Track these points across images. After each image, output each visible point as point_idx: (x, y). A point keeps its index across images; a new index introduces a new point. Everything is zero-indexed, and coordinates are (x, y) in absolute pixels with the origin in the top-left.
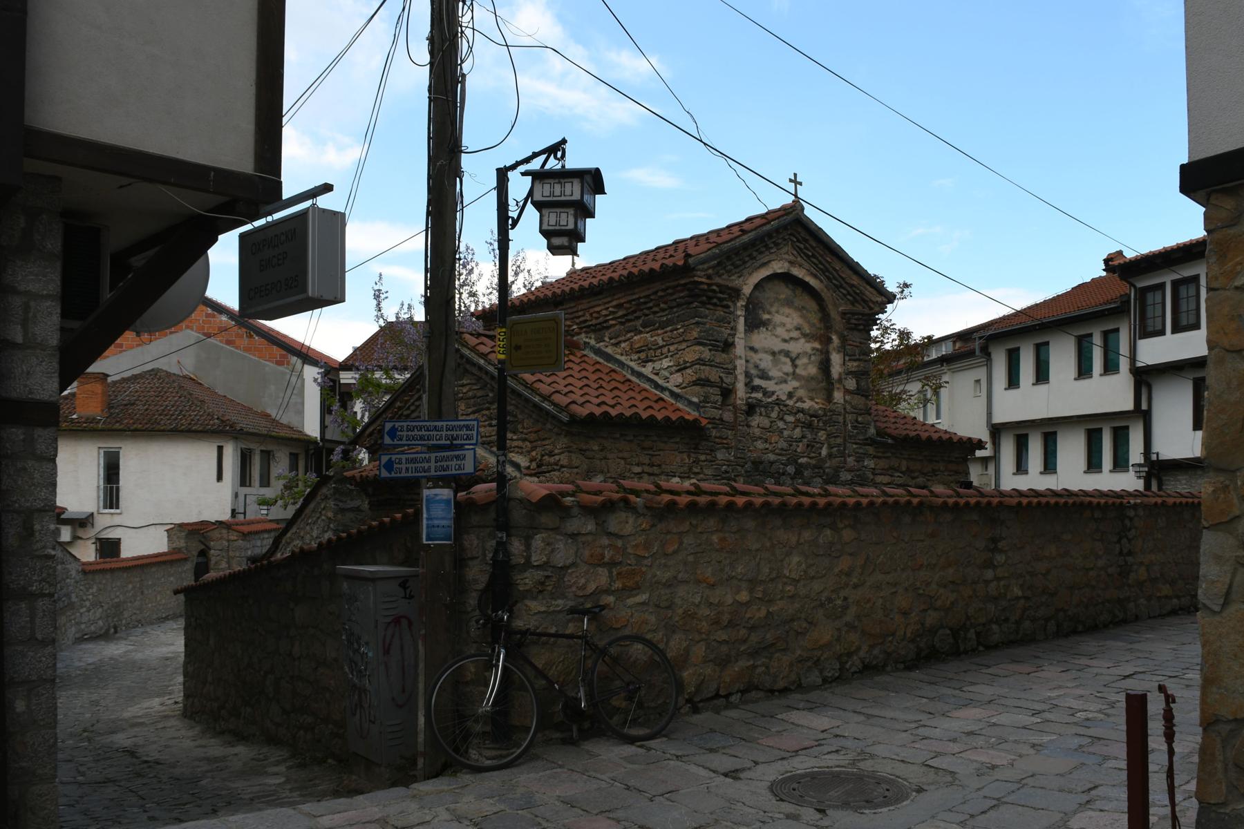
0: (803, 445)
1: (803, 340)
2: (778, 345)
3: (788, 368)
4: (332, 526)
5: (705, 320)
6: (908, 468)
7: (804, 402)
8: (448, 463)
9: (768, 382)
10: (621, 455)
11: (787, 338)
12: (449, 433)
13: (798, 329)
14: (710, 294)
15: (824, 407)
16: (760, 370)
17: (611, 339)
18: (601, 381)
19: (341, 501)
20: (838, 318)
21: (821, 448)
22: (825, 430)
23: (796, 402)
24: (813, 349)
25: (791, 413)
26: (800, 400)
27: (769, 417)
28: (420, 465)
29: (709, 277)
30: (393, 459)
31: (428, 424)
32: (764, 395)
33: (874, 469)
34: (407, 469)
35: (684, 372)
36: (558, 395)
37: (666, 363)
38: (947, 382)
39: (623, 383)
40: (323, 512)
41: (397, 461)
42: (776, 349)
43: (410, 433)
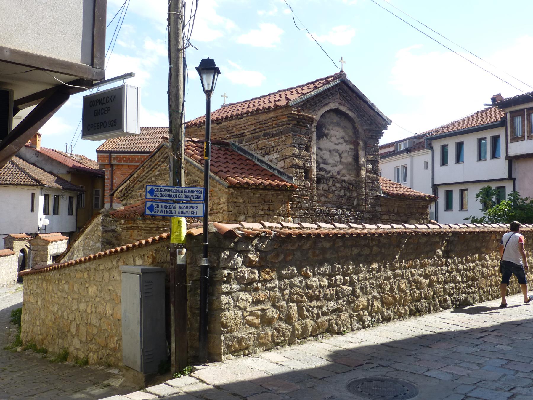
0: (345, 199)
1: (345, 144)
2: (332, 147)
3: (337, 158)
4: (100, 239)
5: (296, 134)
6: (398, 211)
7: (345, 176)
8: (187, 210)
9: (327, 166)
10: (253, 205)
11: (337, 143)
12: (186, 194)
13: (342, 138)
14: (299, 120)
15: (355, 179)
16: (324, 160)
17: (246, 142)
18: (242, 165)
19: (105, 226)
20: (363, 132)
21: (354, 201)
23: (342, 176)
24: (350, 148)
25: (338, 182)
26: (344, 175)
27: (328, 184)
28: (169, 209)
29: (298, 111)
30: (154, 205)
31: (174, 188)
32: (325, 172)
33: (381, 212)
34: (162, 211)
35: (285, 160)
36: (221, 172)
37: (275, 156)
38: (476, 200)
39: (253, 166)
40: (96, 232)
41: (156, 206)
42: (332, 149)
43: (162, 193)
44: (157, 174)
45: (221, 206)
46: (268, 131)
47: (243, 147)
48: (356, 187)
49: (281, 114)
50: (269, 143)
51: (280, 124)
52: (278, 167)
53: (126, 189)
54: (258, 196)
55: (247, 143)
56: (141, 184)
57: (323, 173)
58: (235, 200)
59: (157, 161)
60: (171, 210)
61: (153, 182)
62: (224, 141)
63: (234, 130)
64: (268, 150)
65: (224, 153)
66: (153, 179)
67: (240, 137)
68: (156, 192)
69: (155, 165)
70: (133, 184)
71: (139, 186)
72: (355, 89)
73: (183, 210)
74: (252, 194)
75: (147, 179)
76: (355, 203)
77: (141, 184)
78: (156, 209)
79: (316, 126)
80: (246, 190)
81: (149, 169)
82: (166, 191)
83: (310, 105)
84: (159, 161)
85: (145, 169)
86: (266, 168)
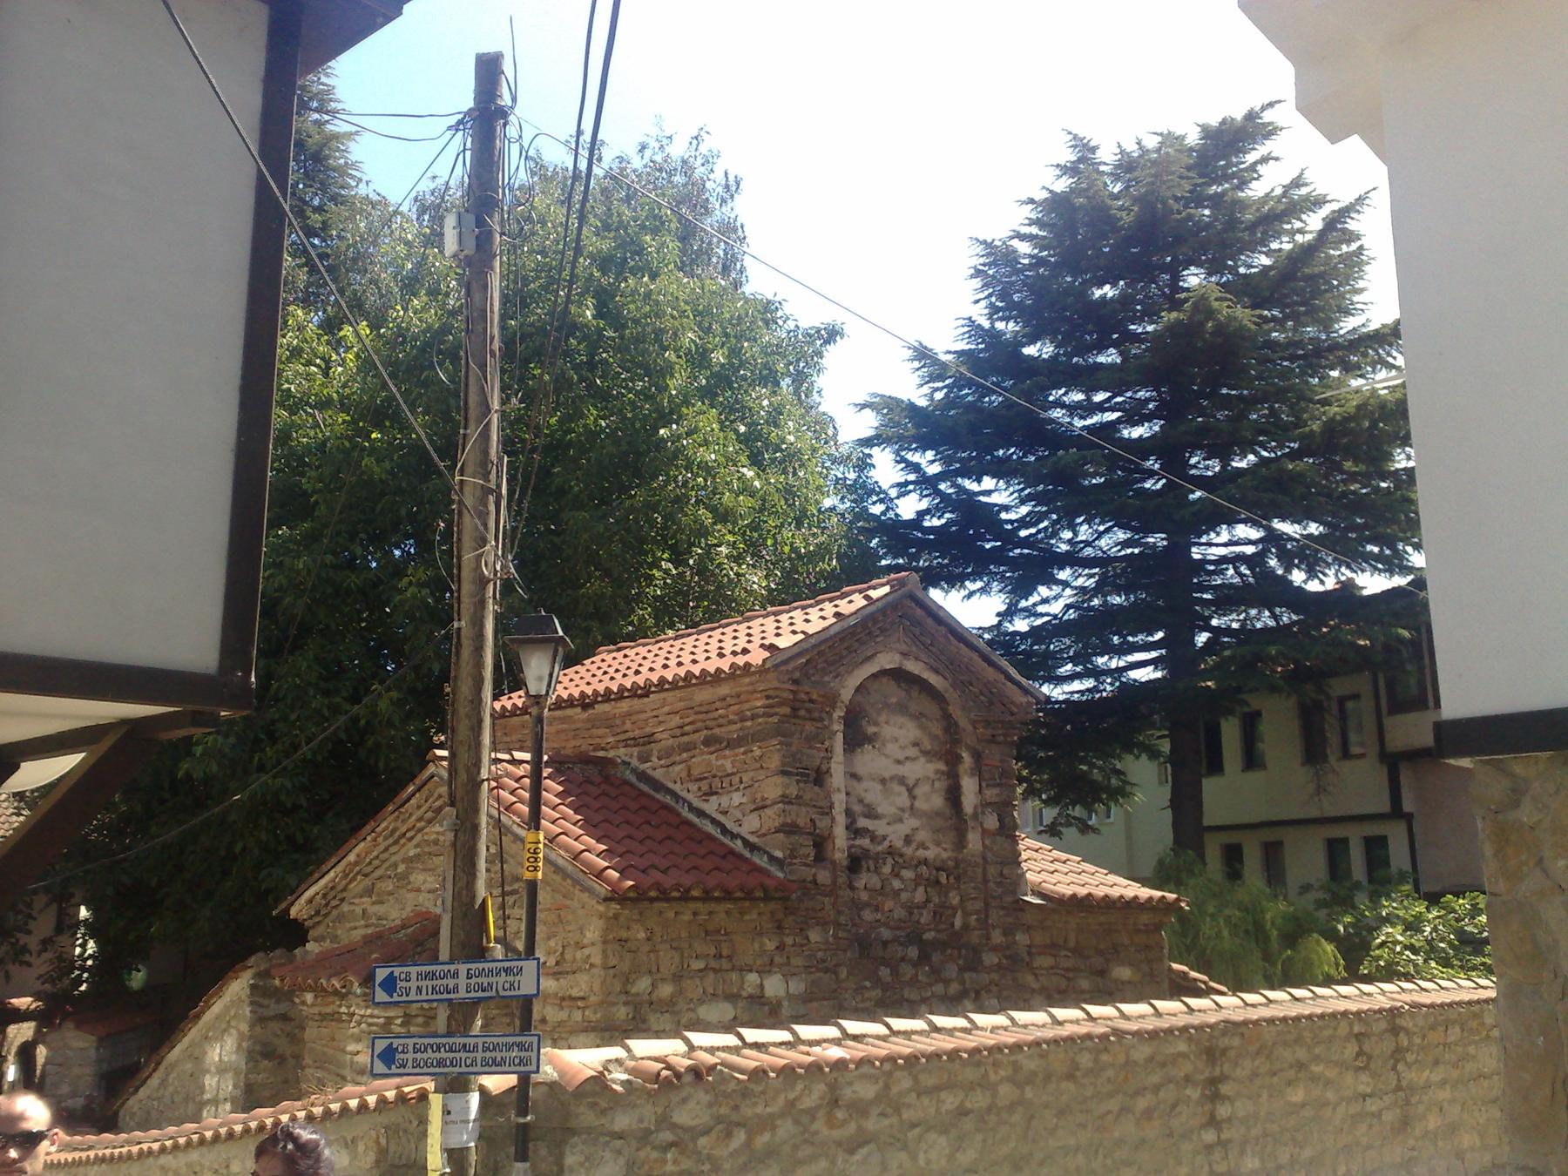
1: (923, 760)
2: (890, 770)
3: (903, 800)
7: (926, 848)
8: (491, 979)
9: (876, 822)
11: (901, 758)
12: (488, 1054)
13: (916, 744)
17: (659, 759)
19: (261, 1006)
20: (970, 728)
21: (954, 916)
22: (958, 888)
26: (923, 846)
28: (439, 982)
30: (396, 974)
31: (451, 1040)
34: (419, 989)
37: (737, 798)
41: (403, 976)
42: (887, 775)
43: (419, 1056)
44: (411, 853)
45: (586, 951)
46: (717, 731)
47: (649, 772)
48: (958, 878)
49: (750, 688)
50: (720, 763)
51: (748, 713)
52: (744, 831)
53: (325, 896)
54: (687, 917)
55: (662, 762)
56: (368, 882)
57: (865, 842)
58: (624, 935)
59: (414, 818)
60: (445, 982)
61: (404, 877)
62: (601, 754)
63: (628, 725)
64: (717, 783)
65: (599, 792)
66: (401, 868)
67: (644, 745)
68: (402, 1056)
69: (408, 830)
70: (344, 882)
71: (361, 886)
72: (941, 613)
73: (479, 980)
74: (671, 914)
75: (385, 866)
76: (958, 923)
77: (368, 882)
78: (404, 984)
79: (843, 718)
80: (656, 905)
81: (391, 840)
82: (429, 1050)
83: (826, 661)
84: (420, 819)
85: (380, 839)
86: (713, 832)
